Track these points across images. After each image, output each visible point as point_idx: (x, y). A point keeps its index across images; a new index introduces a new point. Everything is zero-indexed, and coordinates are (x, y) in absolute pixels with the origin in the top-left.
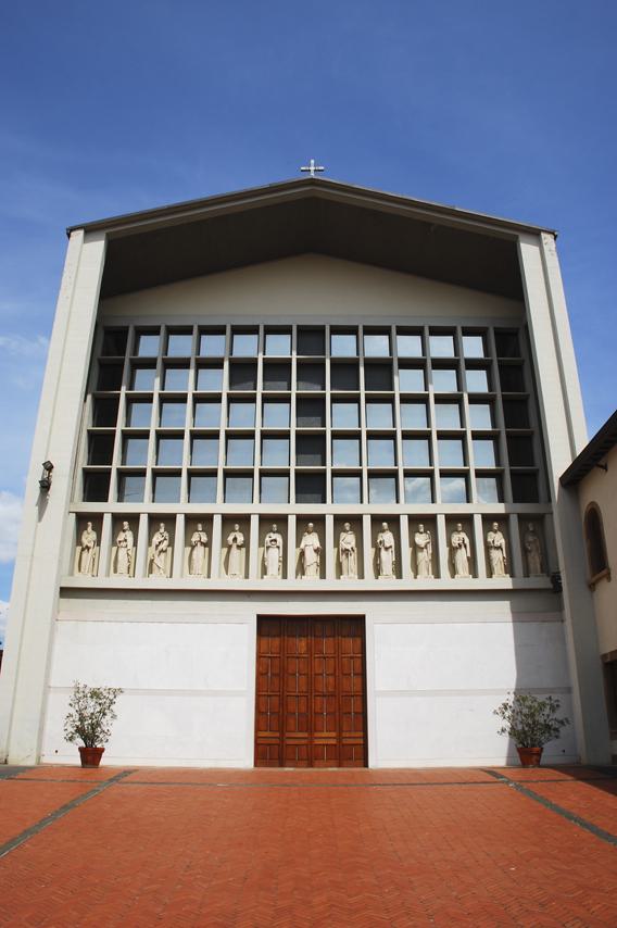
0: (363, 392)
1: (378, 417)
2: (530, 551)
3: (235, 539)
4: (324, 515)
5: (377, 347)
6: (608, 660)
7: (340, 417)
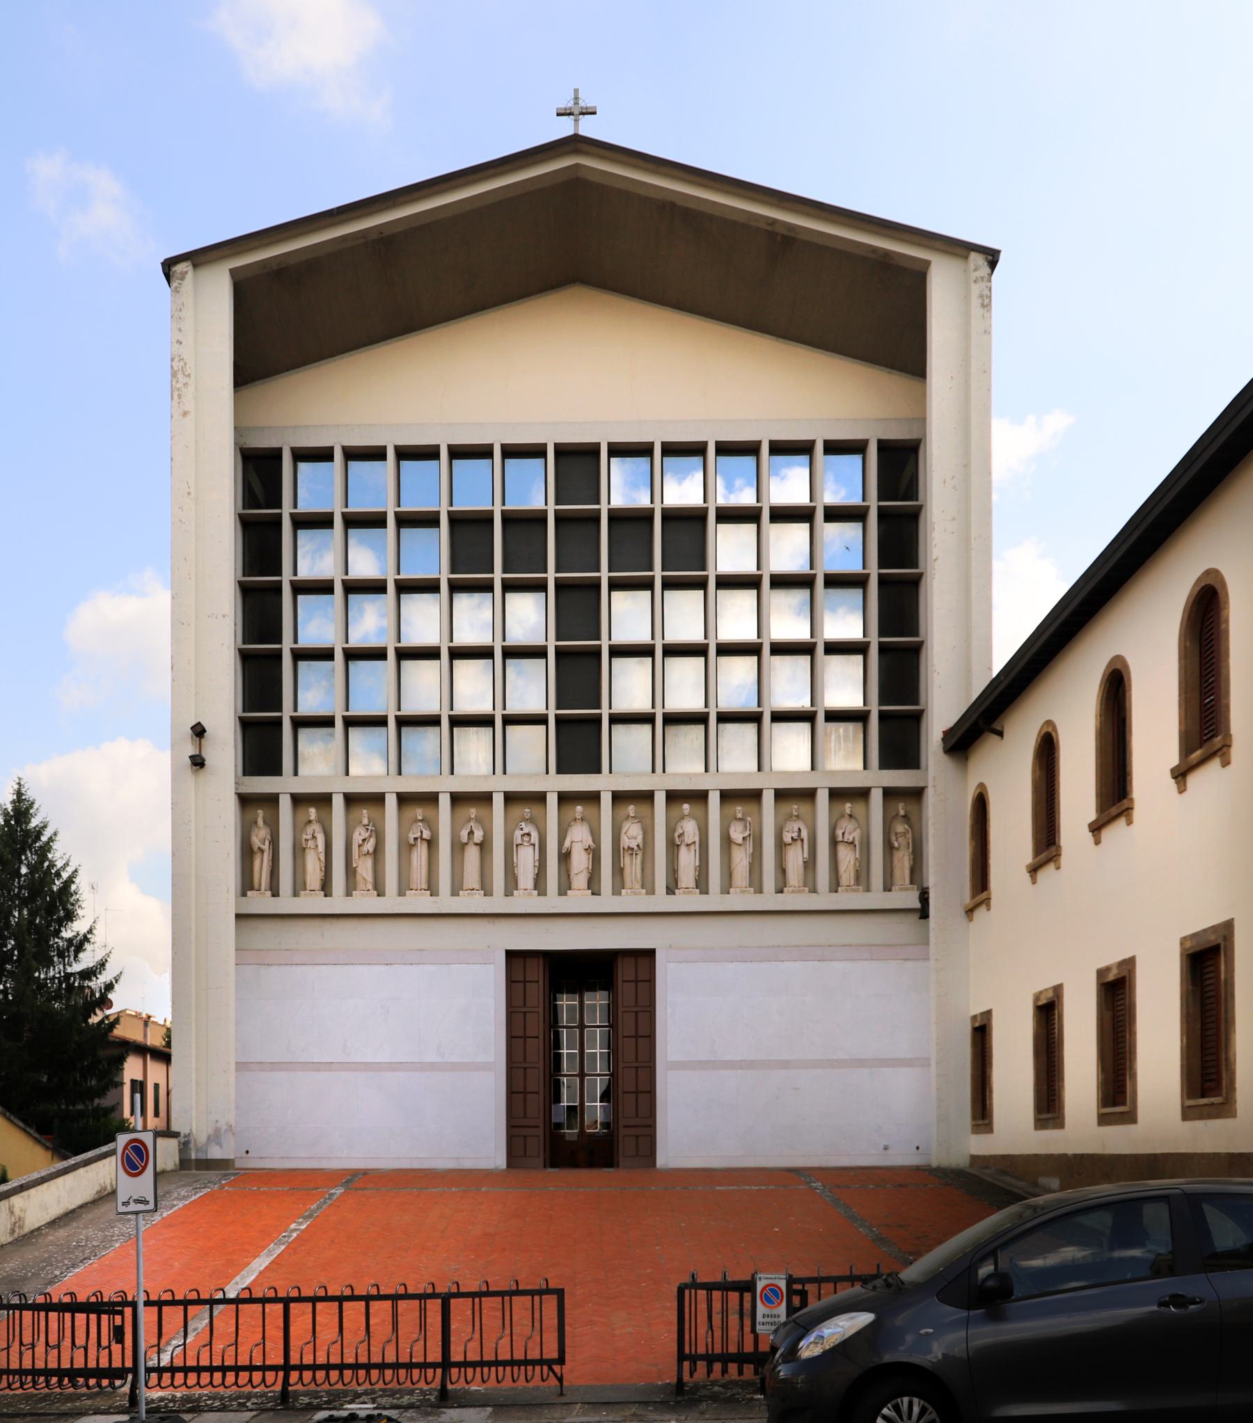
0: (658, 573)
1: (684, 617)
2: (898, 849)
3: (471, 833)
4: (599, 792)
5: (683, 489)
6: (1111, 977)
7: (627, 616)
